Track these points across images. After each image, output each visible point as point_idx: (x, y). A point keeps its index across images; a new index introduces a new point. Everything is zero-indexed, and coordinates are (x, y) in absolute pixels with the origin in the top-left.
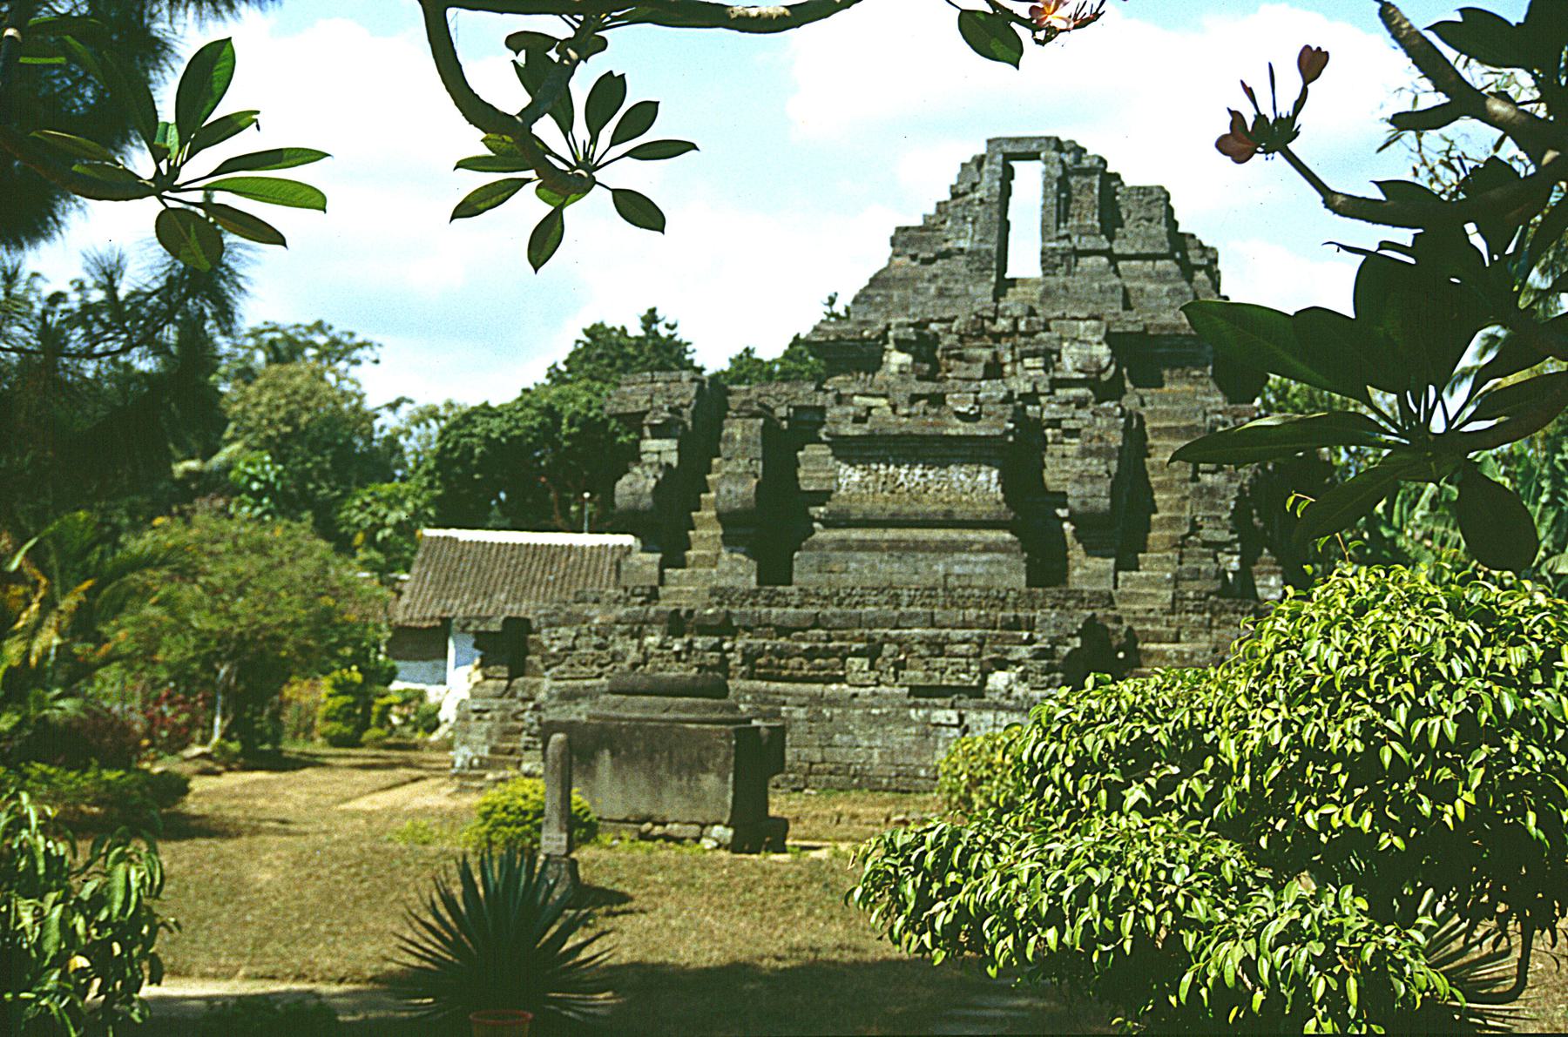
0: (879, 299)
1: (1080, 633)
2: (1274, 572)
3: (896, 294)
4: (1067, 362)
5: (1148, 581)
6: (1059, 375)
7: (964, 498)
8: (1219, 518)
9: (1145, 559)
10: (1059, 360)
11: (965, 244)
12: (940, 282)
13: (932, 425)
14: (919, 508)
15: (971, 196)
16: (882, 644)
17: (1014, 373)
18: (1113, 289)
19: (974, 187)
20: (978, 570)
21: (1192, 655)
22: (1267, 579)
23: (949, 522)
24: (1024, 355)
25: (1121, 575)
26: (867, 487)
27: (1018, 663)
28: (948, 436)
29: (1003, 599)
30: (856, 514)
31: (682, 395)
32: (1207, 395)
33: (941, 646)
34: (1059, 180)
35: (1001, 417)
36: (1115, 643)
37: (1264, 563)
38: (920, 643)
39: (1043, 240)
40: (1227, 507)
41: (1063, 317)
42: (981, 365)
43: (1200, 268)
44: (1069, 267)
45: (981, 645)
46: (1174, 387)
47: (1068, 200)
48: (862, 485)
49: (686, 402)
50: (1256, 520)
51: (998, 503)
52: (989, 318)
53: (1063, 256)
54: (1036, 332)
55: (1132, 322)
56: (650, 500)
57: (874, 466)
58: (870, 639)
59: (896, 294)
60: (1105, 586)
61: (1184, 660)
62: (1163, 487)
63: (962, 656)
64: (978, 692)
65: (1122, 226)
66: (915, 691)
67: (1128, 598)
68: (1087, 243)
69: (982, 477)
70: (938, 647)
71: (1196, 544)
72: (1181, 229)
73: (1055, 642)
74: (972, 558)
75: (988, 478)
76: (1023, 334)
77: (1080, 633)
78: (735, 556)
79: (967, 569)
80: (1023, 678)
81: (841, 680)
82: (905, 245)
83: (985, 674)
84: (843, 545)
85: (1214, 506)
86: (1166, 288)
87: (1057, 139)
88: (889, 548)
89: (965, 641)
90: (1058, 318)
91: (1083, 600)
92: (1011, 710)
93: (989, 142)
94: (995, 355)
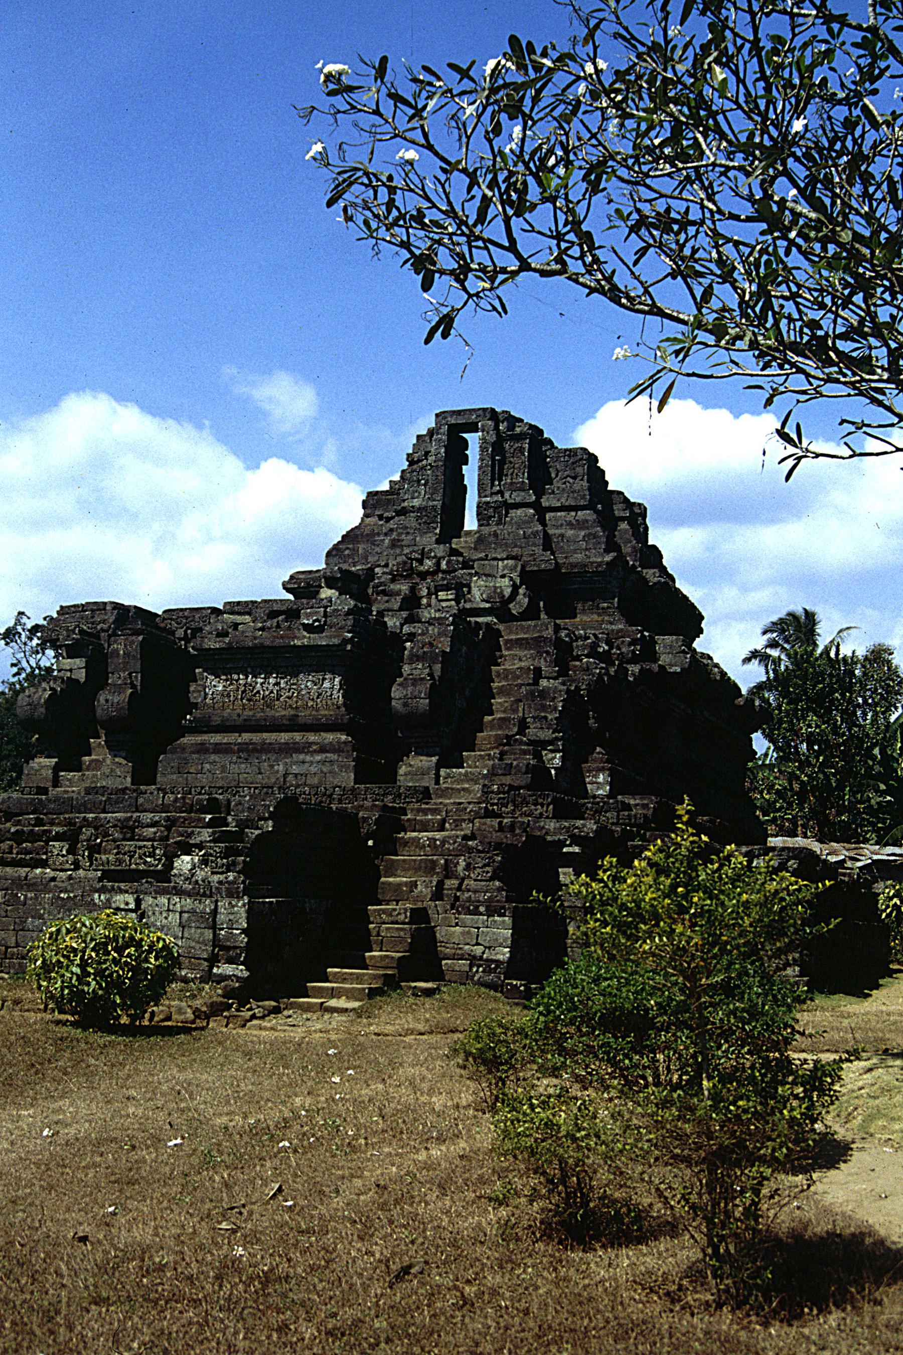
0: (347, 552)
1: (272, 816)
2: (602, 770)
3: (361, 548)
4: (476, 593)
5: (467, 777)
6: (468, 606)
7: (310, 703)
8: (546, 718)
9: (468, 757)
10: (469, 592)
11: (416, 503)
12: (394, 535)
13: (282, 637)
14: (269, 713)
15: (424, 462)
16: (81, 828)
17: (429, 605)
18: (535, 534)
19: (427, 454)
20: (313, 769)
21: (443, 842)
22: (596, 776)
23: (293, 725)
24: (438, 589)
25: (443, 772)
26: (229, 696)
27: (200, 846)
28: (295, 646)
29: (330, 796)
30: (216, 720)
31: (104, 622)
32: (611, 623)
33: (132, 829)
34: (493, 445)
35: (342, 628)
36: (364, 831)
37: (595, 761)
38: (115, 826)
39: (480, 496)
40: (555, 708)
41: (486, 558)
42: (399, 598)
43: (623, 519)
44: (500, 519)
45: (168, 828)
46: (585, 618)
47: (502, 463)
48: (225, 694)
49: (105, 626)
50: (591, 721)
51: (338, 708)
52: (417, 560)
53: (495, 508)
54: (455, 570)
55: (544, 560)
56: (43, 710)
57: (235, 677)
58: (71, 823)
59: (361, 548)
60: (428, 782)
61: (436, 847)
62: (502, 691)
63: (148, 840)
64: (165, 875)
65: (551, 484)
66: (107, 875)
67: (444, 793)
68: (517, 497)
69: (327, 684)
70: (129, 830)
71: (521, 743)
72: (610, 488)
73: (243, 825)
74: (308, 758)
75: (332, 685)
76: (444, 572)
77: (272, 816)
78: (117, 760)
79: (303, 769)
80: (204, 862)
81: (44, 864)
82: (374, 507)
83: (170, 858)
84: (202, 749)
85: (544, 708)
86: (583, 533)
87: (493, 410)
88: (239, 751)
89: (154, 824)
90: (481, 559)
91: (399, 795)
92: (189, 894)
93: (437, 415)
94: (413, 589)
